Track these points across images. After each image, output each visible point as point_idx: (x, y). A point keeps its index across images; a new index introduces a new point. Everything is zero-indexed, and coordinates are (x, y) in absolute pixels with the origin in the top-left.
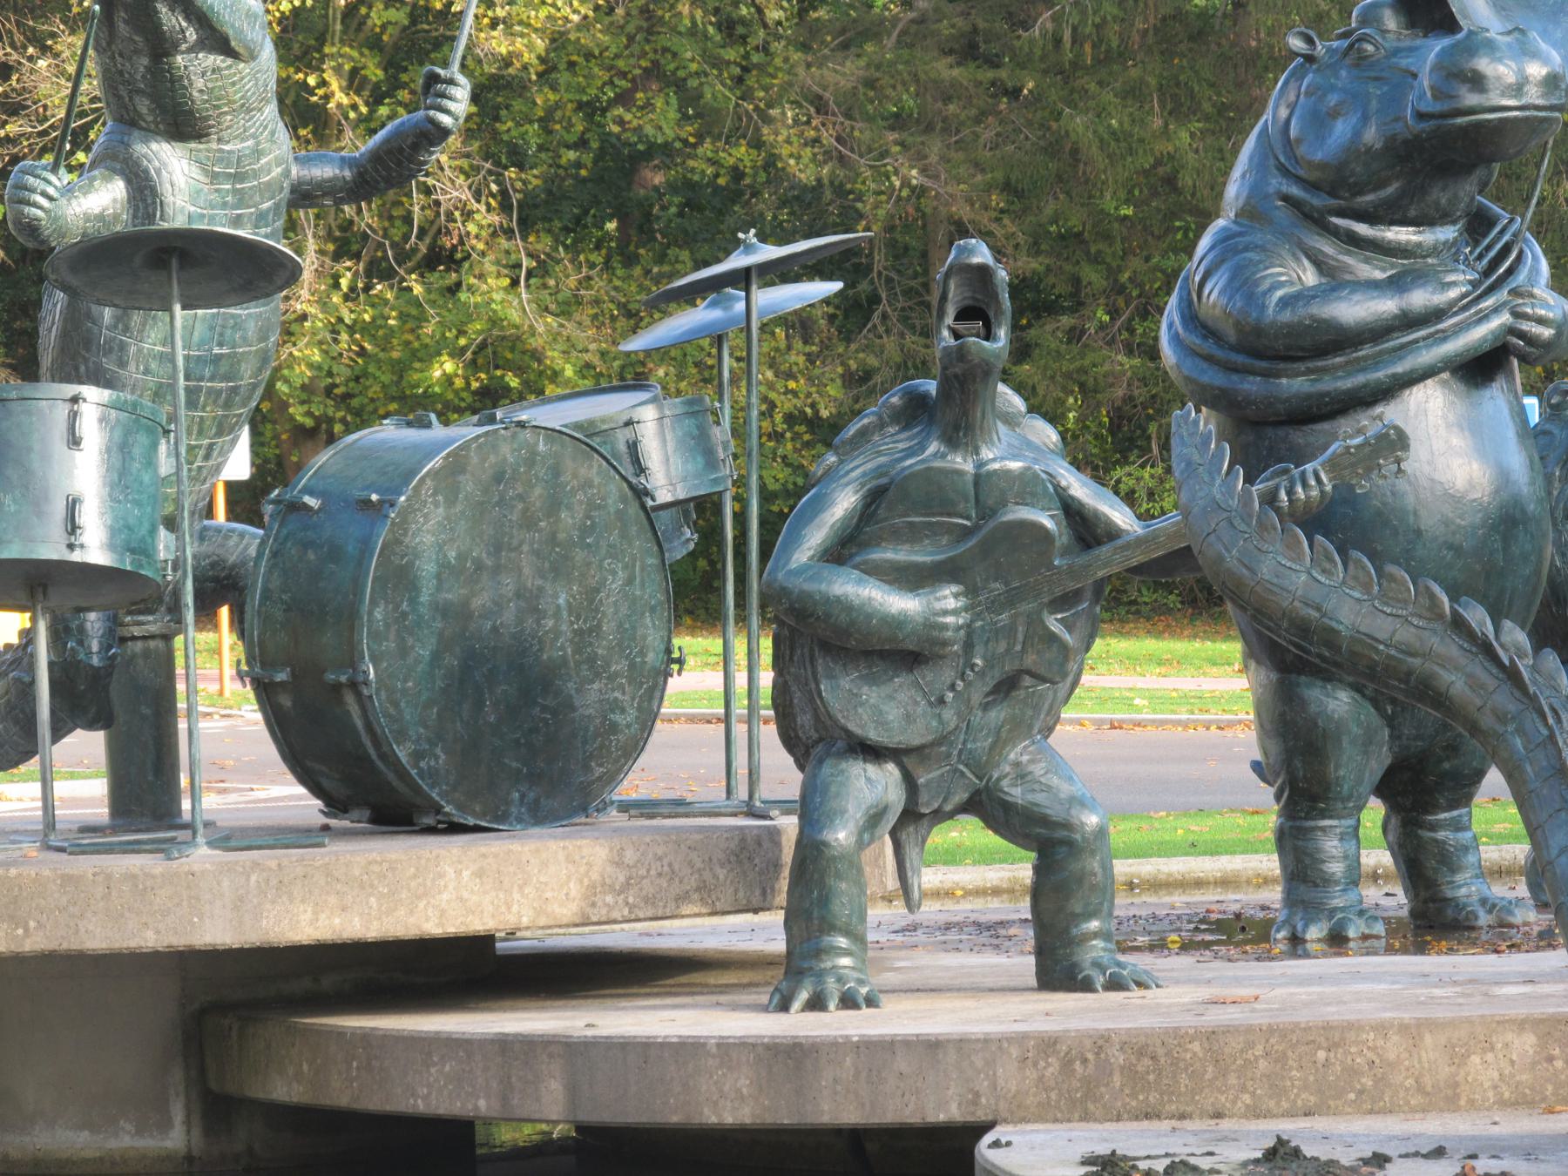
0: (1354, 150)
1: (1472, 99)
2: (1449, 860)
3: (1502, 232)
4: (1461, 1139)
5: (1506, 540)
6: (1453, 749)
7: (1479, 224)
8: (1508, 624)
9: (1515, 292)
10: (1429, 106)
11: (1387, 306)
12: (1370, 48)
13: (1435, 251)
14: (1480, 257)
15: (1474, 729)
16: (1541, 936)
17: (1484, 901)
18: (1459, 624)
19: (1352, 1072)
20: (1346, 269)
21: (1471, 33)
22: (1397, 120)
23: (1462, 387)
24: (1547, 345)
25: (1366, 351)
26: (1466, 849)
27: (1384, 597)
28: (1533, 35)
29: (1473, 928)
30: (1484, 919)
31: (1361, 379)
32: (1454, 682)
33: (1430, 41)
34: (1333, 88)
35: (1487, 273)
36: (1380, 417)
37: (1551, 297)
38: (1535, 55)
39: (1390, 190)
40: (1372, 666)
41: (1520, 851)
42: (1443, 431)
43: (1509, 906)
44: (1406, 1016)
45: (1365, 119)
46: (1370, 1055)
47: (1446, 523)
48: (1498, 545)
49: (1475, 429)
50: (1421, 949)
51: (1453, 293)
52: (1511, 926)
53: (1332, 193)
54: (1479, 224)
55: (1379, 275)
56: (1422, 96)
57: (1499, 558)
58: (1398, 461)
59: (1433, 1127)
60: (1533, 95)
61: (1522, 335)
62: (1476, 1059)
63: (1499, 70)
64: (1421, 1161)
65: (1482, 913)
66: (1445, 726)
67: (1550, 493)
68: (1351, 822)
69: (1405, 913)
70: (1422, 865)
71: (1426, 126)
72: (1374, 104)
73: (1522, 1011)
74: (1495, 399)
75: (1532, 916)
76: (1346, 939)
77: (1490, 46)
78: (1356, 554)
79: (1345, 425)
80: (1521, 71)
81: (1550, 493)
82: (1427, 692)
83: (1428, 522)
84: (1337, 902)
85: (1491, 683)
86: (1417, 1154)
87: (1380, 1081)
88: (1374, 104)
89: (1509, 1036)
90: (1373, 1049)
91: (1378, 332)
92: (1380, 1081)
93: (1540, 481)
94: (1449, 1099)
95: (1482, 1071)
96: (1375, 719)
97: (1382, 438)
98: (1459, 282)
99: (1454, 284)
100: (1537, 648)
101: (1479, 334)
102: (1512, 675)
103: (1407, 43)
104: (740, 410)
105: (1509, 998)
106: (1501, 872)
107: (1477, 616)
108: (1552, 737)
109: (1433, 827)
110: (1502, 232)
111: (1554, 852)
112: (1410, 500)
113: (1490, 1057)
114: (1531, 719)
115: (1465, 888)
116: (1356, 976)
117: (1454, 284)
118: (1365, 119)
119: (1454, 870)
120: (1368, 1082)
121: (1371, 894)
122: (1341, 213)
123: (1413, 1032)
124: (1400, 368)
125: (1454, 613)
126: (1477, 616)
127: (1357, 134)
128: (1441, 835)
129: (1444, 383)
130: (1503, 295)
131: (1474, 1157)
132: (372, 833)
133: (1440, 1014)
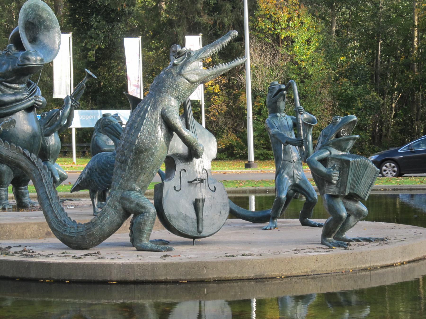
0: (7, 71)
1: (27, 63)
2: (23, 195)
3: (33, 86)
4: (24, 244)
5: (34, 139)
6: (24, 176)
7: (29, 84)
8: (32, 154)
9: (35, 96)
10: (20, 63)
11: (13, 98)
12: (10, 53)
13: (21, 89)
14: (29, 90)
15: (27, 172)
16: (39, 208)
17: (30, 202)
18: (24, 154)
19: (5, 232)
20: (6, 91)
21: (27, 51)
22: (15, 65)
23: (26, 113)
24: (41, 106)
25: (9, 106)
26: (27, 193)
27: (11, 149)
28: (38, 52)
29: (28, 207)
30: (30, 205)
31: (8, 111)
32: (23, 164)
33: (21, 52)
34: (3, 60)
35: (30, 93)
36: (11, 118)
37: (42, 97)
38: (39, 55)
39: (14, 78)
40: (9, 161)
41: (35, 194)
42: (23, 120)
43: (34, 203)
44: (15, 222)
45: (9, 65)
46: (9, 229)
47: (23, 136)
48: (32, 140)
49: (28, 120)
50: (18, 211)
51: (24, 96)
52: (34, 207)
53: (3, 78)
54: (29, 84)
55: (11, 93)
56: (19, 62)
57: (33, 143)
58: (14, 125)
59: (20, 242)
60: (38, 62)
61: (36, 104)
62: (27, 230)
63: (33, 58)
64: (17, 248)
65: (29, 204)
66: (23, 172)
67: (41, 131)
68: (6, 188)
69: (16, 204)
70: (19, 196)
71: (19, 67)
72: (11, 63)
73: (35, 221)
74: (32, 114)
75: (38, 205)
76: (5, 209)
77: (31, 53)
78: (6, 141)
79: (5, 119)
80: (36, 58)
81: (41, 131)
82: (18, 166)
83: (20, 136)
84: (4, 203)
85: (30, 164)
86: (16, 246)
87: (10, 234)
88: (11, 63)
89: (33, 226)
90: (9, 228)
91: (11, 103)
92: (10, 234)
93: (40, 129)
94: (22, 237)
95: (28, 232)
96: (11, 171)
97: (11, 121)
98: (25, 95)
99: (25, 95)
100: (38, 158)
101: (29, 103)
102: (33, 163)
103: (16, 52)
104: (96, 176)
105: (33, 219)
106: (34, 197)
107: (27, 153)
108: (40, 174)
109: (21, 189)
110: (33, 86)
111: (40, 194)
112: (17, 132)
113: (29, 229)
114: (36, 170)
115: (26, 200)
116: (7, 215)
117: (25, 95)
118: (9, 65)
119: (24, 197)
120: (8, 234)
121: (10, 201)
122: (5, 82)
123: (16, 225)
124: (15, 109)
125: (23, 152)
126: (27, 153)
127: (8, 68)
128: (22, 191)
129: (23, 112)
130: (33, 97)
131: (26, 247)
132: (69, 249)
133: (21, 222)
